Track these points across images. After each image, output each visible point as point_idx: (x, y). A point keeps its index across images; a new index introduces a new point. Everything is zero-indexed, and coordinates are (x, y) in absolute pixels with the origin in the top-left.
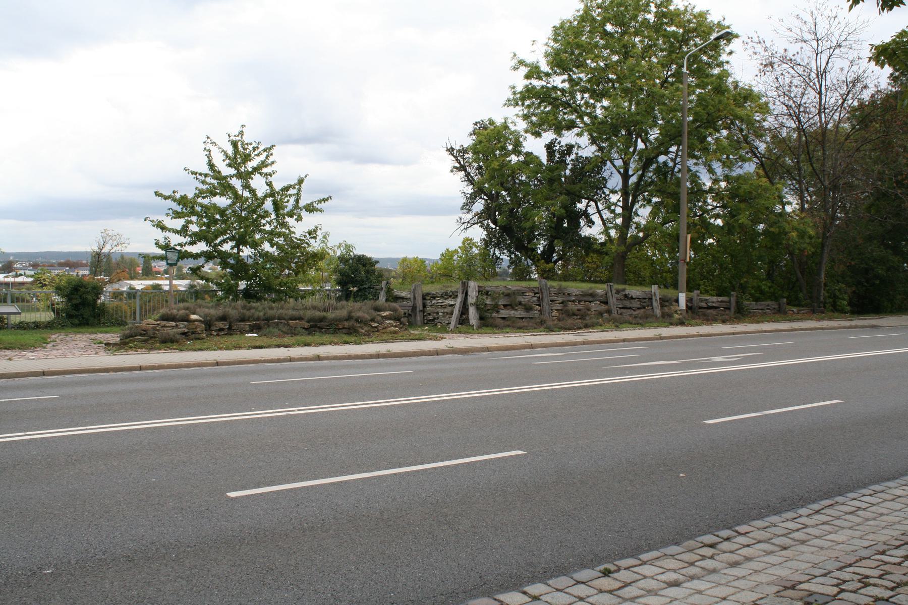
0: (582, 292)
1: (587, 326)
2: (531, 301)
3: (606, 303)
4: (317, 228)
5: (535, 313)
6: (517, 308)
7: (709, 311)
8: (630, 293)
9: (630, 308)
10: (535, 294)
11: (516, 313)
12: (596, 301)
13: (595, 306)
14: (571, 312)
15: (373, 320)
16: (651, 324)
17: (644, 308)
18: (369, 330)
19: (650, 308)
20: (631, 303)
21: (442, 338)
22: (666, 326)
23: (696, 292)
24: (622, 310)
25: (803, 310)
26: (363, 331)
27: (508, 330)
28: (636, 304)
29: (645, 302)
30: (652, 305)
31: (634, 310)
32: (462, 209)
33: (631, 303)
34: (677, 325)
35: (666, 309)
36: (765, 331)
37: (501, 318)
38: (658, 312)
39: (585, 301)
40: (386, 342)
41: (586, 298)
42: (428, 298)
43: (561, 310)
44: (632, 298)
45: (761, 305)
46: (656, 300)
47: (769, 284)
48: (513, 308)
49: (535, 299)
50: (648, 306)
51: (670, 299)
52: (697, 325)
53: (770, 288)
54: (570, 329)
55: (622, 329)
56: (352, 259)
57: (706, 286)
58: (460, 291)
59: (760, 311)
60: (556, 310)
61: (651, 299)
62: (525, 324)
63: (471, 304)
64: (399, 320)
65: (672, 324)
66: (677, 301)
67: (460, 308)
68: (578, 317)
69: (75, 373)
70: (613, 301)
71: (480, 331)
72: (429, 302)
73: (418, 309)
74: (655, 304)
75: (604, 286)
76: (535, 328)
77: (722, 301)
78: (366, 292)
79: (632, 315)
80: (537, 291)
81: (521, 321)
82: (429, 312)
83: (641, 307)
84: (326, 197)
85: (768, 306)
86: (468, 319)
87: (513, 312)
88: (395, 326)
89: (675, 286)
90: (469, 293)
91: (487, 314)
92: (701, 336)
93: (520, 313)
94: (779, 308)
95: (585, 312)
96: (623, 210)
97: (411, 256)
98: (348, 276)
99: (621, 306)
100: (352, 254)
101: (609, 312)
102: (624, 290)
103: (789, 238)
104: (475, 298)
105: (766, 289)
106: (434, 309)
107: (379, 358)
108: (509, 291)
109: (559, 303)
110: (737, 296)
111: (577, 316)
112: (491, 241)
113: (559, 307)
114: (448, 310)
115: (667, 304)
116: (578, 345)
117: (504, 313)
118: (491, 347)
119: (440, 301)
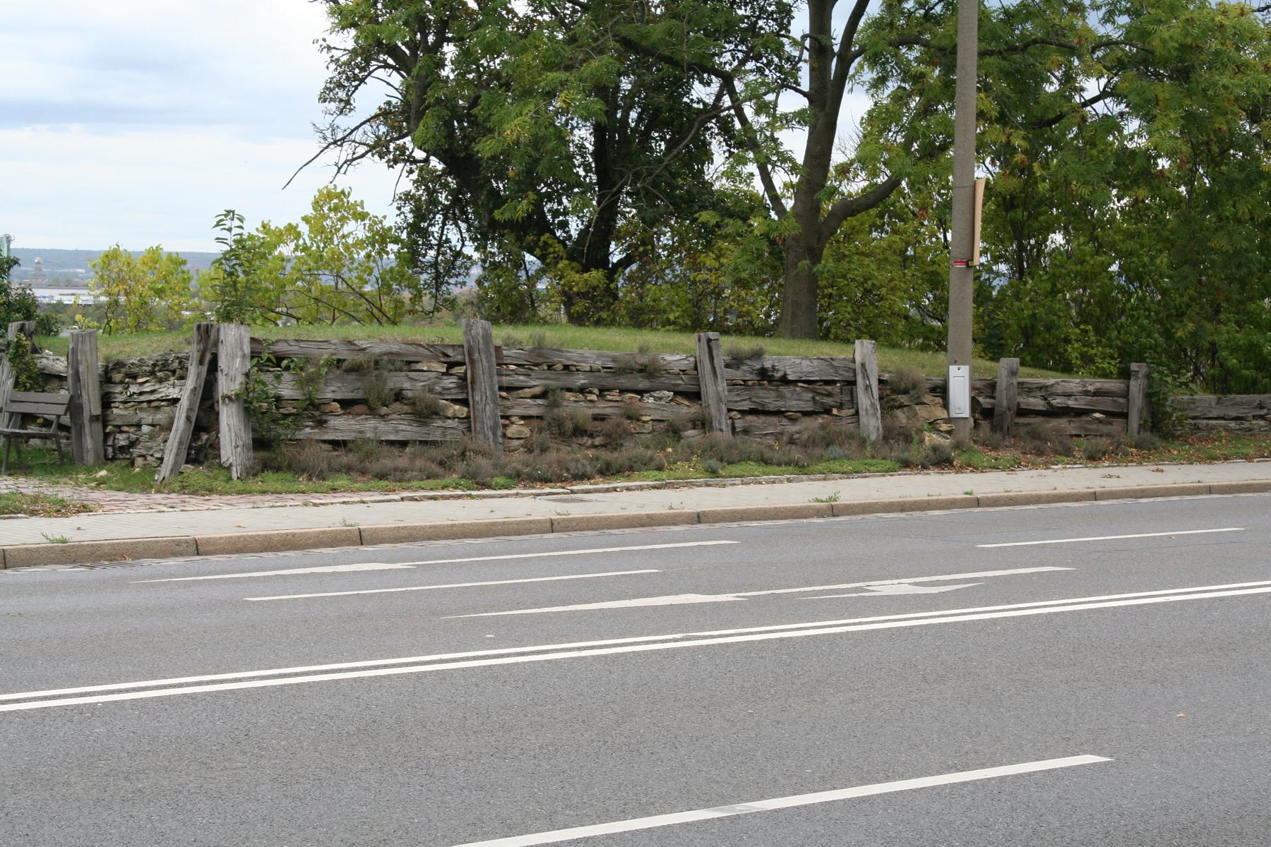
1: (608, 471)
2: (438, 388)
5: (446, 429)
6: (384, 410)
7: (1055, 423)
8: (779, 366)
9: (778, 413)
10: (451, 365)
11: (382, 426)
12: (660, 389)
13: (655, 406)
14: (569, 426)
16: (835, 465)
17: (828, 411)
20: (781, 397)
21: (85, 509)
22: (889, 471)
24: (750, 418)
27: (342, 481)
28: (797, 400)
29: (829, 395)
30: (853, 401)
31: (793, 420)
33: (781, 397)
34: (924, 467)
35: (901, 417)
36: (1210, 490)
37: (325, 442)
38: (872, 424)
39: (622, 391)
41: (624, 381)
42: (117, 377)
43: (540, 418)
44: (784, 381)
45: (1235, 404)
46: (868, 387)
48: (372, 412)
49: (450, 382)
51: (915, 386)
52: (996, 468)
54: (545, 480)
55: (729, 481)
57: (1087, 344)
58: (193, 351)
59: (1232, 424)
60: (523, 417)
61: (853, 383)
62: (402, 462)
63: (224, 397)
65: (906, 465)
66: (941, 390)
67: (190, 409)
68: (598, 441)
70: (715, 389)
71: (255, 484)
72: (119, 389)
73: (86, 415)
74: (864, 401)
77: (1097, 393)
79: (781, 434)
80: (459, 358)
81: (396, 451)
86: (215, 446)
87: (372, 423)
89: (936, 342)
90: (222, 363)
91: (280, 431)
92: (978, 503)
93: (399, 427)
95: (618, 425)
97: (136, 243)
99: (746, 406)
101: (702, 423)
102: (758, 355)
107: (699, 522)
108: (360, 358)
109: (534, 397)
111: (591, 436)
112: (433, 201)
113: (534, 407)
114: (161, 417)
115: (903, 399)
116: (529, 532)
117: (343, 426)
118: (209, 541)
119: (147, 388)
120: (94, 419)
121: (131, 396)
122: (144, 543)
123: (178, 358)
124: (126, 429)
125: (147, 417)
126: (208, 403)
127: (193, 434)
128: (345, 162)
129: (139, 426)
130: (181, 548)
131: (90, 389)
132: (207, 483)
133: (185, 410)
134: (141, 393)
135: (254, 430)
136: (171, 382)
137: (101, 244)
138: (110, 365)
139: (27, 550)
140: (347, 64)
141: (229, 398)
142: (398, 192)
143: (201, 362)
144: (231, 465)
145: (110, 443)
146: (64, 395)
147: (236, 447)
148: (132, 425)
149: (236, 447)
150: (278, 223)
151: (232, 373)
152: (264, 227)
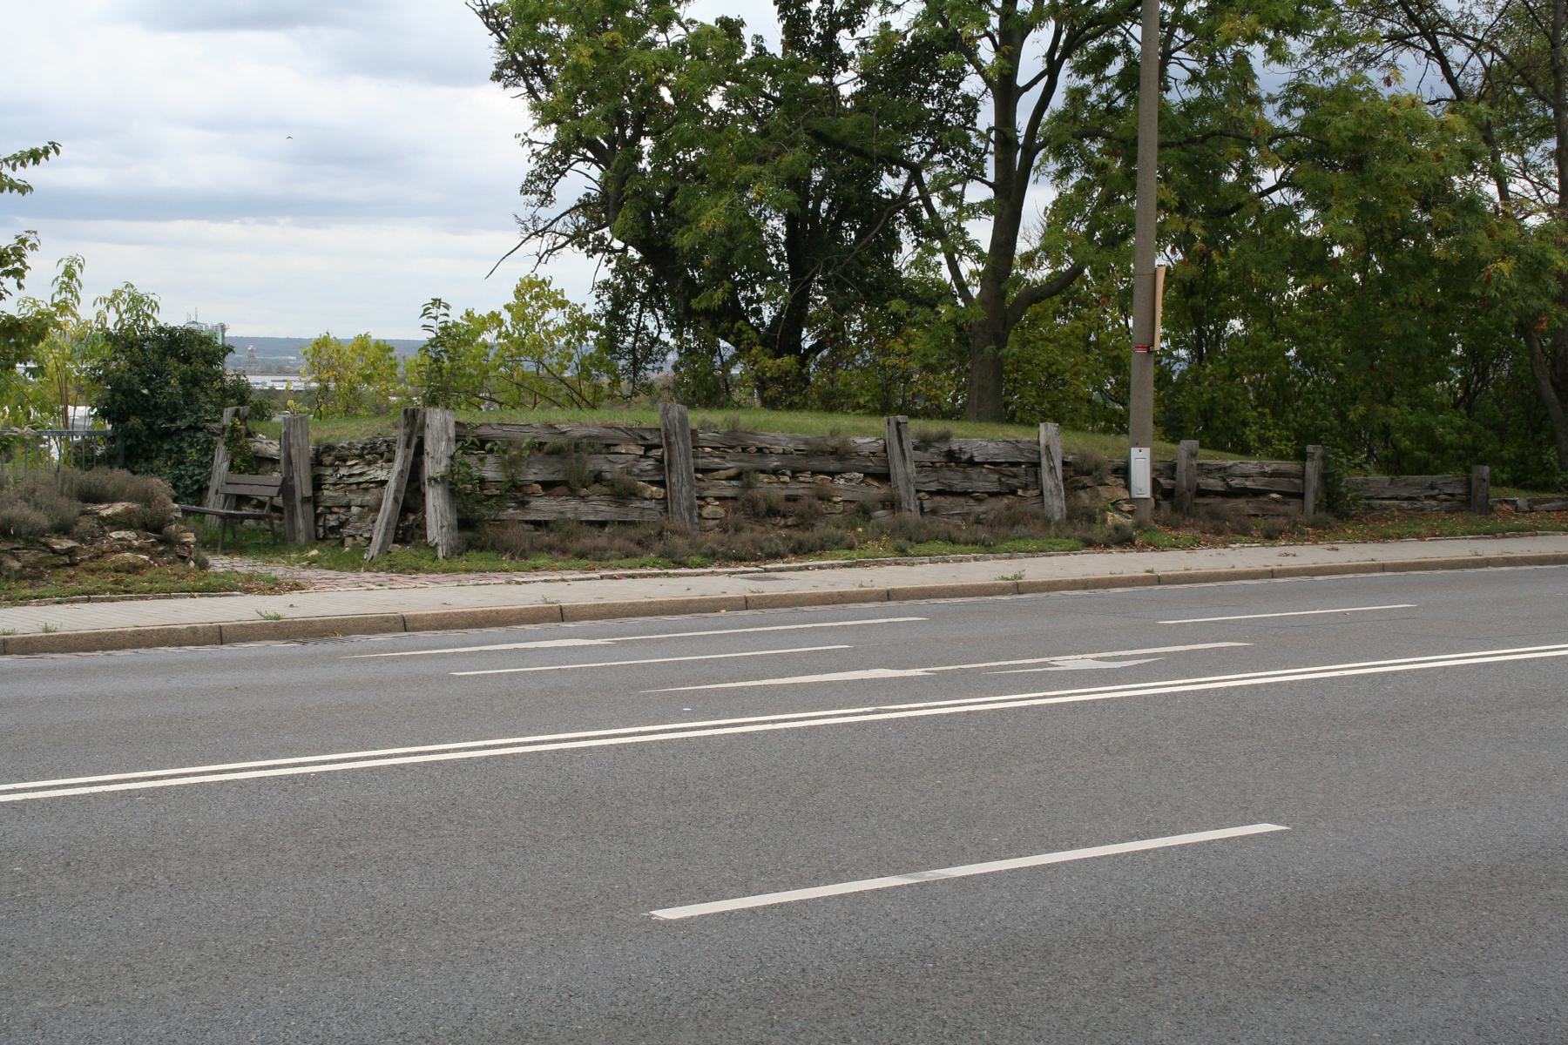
0: (806, 442)
1: (801, 550)
2: (636, 470)
3: (884, 477)
4: (23, 241)
5: (644, 510)
6: (584, 491)
7: (1232, 503)
8: (966, 448)
9: (965, 494)
10: (648, 448)
11: (582, 507)
13: (845, 487)
14: (763, 506)
15: (64, 530)
16: (1021, 544)
17: (1014, 492)
18: (40, 562)
19: (1032, 492)
20: (968, 478)
21: (297, 587)
23: (1187, 445)
24: (937, 499)
25: (1548, 501)
26: (16, 565)
28: (984, 481)
29: (1015, 476)
30: (1038, 482)
31: (979, 500)
32: (524, 191)
33: (968, 478)
34: (1107, 546)
35: (1085, 497)
36: (1383, 568)
37: (527, 522)
38: (1056, 505)
39: (814, 473)
40: (88, 600)
41: (815, 463)
42: (328, 460)
43: (734, 498)
44: (971, 462)
46: (1052, 469)
47: (1459, 422)
48: (573, 493)
49: (647, 464)
50: (1026, 487)
51: (1097, 468)
52: (1175, 547)
53: (1459, 431)
54: (740, 559)
55: (917, 559)
56: (155, 339)
58: (399, 434)
59: (1405, 504)
60: (717, 498)
61: (1038, 465)
62: (602, 541)
63: (430, 479)
64: (158, 530)
65: (1089, 544)
66: (1124, 472)
69: (930, 597)
70: (904, 471)
72: (329, 471)
73: (298, 496)
74: (1048, 482)
75: (879, 424)
76: (634, 555)
77: (1275, 474)
78: (182, 440)
79: (968, 514)
80: (656, 441)
81: (595, 531)
82: (329, 504)
83: (1005, 490)
84: (41, 147)
85: (1432, 487)
86: (421, 526)
87: (573, 503)
88: (140, 550)
89: (1118, 424)
90: (428, 446)
92: (1159, 580)
94: (1469, 493)
96: (996, 193)
97: (345, 331)
98: (131, 393)
99: (934, 487)
100: (151, 324)
101: (892, 504)
102: (945, 437)
103: (1489, 278)
104: (445, 462)
105: (1448, 438)
106: (341, 493)
107: (889, 600)
108: (561, 441)
109: (729, 478)
110: (1324, 458)
111: (784, 516)
112: (630, 289)
114: (369, 498)
115: (1086, 480)
117: (544, 507)
118: (416, 618)
119: (357, 470)
120: (305, 500)
124: (336, 510)
125: (356, 499)
127: (401, 515)
129: (348, 507)
132: (414, 562)
134: (351, 476)
135: (459, 511)
136: (379, 465)
141: (435, 480)
146: (276, 477)
147: (442, 527)
150: (482, 311)
151: (438, 456)
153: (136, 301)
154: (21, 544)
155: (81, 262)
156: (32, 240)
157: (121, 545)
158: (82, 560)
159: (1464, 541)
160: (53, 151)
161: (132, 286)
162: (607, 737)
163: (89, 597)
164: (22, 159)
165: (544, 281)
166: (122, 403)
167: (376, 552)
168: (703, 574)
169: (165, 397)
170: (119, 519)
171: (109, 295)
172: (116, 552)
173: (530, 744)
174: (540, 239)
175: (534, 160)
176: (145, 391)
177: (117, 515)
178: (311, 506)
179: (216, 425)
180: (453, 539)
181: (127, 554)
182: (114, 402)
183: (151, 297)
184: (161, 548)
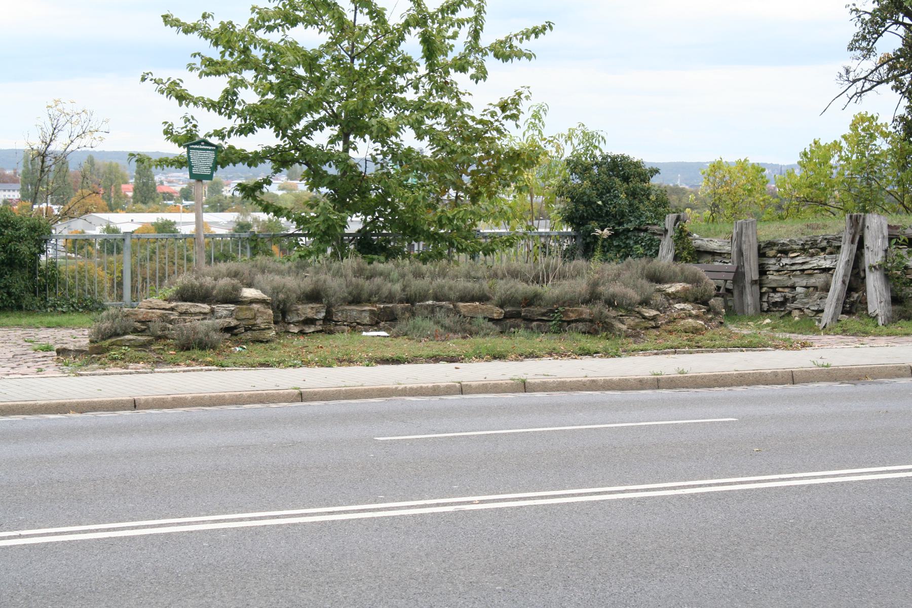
4: (519, 94)
15: (645, 303)
18: (637, 325)
21: (804, 345)
26: (624, 327)
32: (851, 49)
40: (675, 352)
42: (771, 253)
63: (871, 267)
64: (705, 303)
71: (892, 328)
72: (773, 261)
73: (748, 279)
82: (774, 285)
84: (540, 26)
86: (864, 302)
88: (697, 317)
90: (868, 242)
97: (731, 157)
98: (589, 203)
100: (597, 153)
106: (785, 277)
107: (658, 388)
114: (819, 280)
119: (799, 260)
120: (754, 282)
121: (783, 266)
122: (878, 368)
123: (826, 239)
124: (780, 289)
125: (801, 281)
126: (857, 271)
127: (847, 293)
128: (856, 94)
129: (793, 288)
130: (901, 372)
131: (752, 261)
132: (862, 328)
133: (841, 276)
134: (793, 264)
135: (892, 291)
136: (823, 256)
137: (708, 157)
138: (763, 245)
139: (806, 371)
140: (872, 21)
141: (875, 267)
142: (898, 114)
143: (853, 242)
144: (877, 315)
145: (765, 299)
146: (731, 266)
147: (881, 302)
148: (787, 287)
149: (881, 302)
150: (826, 140)
151: (876, 250)
152: (815, 143)
153: (589, 139)
154: (623, 312)
155: (546, 107)
156: (526, 93)
157: (685, 313)
158: (662, 324)
159: (224, 372)
160: (548, 28)
161: (583, 125)
162: (542, 497)
163: (675, 350)
164: (527, 35)
165: (872, 117)
166: (583, 212)
167: (829, 321)
168: (189, 371)
169: (615, 207)
170: (678, 295)
171: (566, 133)
172: (683, 319)
173: (723, 484)
174: (847, 84)
175: (859, 24)
176: (600, 203)
177: (677, 292)
178: (758, 287)
179: (657, 227)
180: (889, 311)
181: (690, 320)
182: (577, 211)
183: (599, 133)
184: (710, 316)
